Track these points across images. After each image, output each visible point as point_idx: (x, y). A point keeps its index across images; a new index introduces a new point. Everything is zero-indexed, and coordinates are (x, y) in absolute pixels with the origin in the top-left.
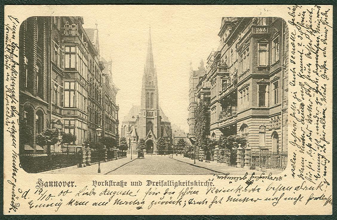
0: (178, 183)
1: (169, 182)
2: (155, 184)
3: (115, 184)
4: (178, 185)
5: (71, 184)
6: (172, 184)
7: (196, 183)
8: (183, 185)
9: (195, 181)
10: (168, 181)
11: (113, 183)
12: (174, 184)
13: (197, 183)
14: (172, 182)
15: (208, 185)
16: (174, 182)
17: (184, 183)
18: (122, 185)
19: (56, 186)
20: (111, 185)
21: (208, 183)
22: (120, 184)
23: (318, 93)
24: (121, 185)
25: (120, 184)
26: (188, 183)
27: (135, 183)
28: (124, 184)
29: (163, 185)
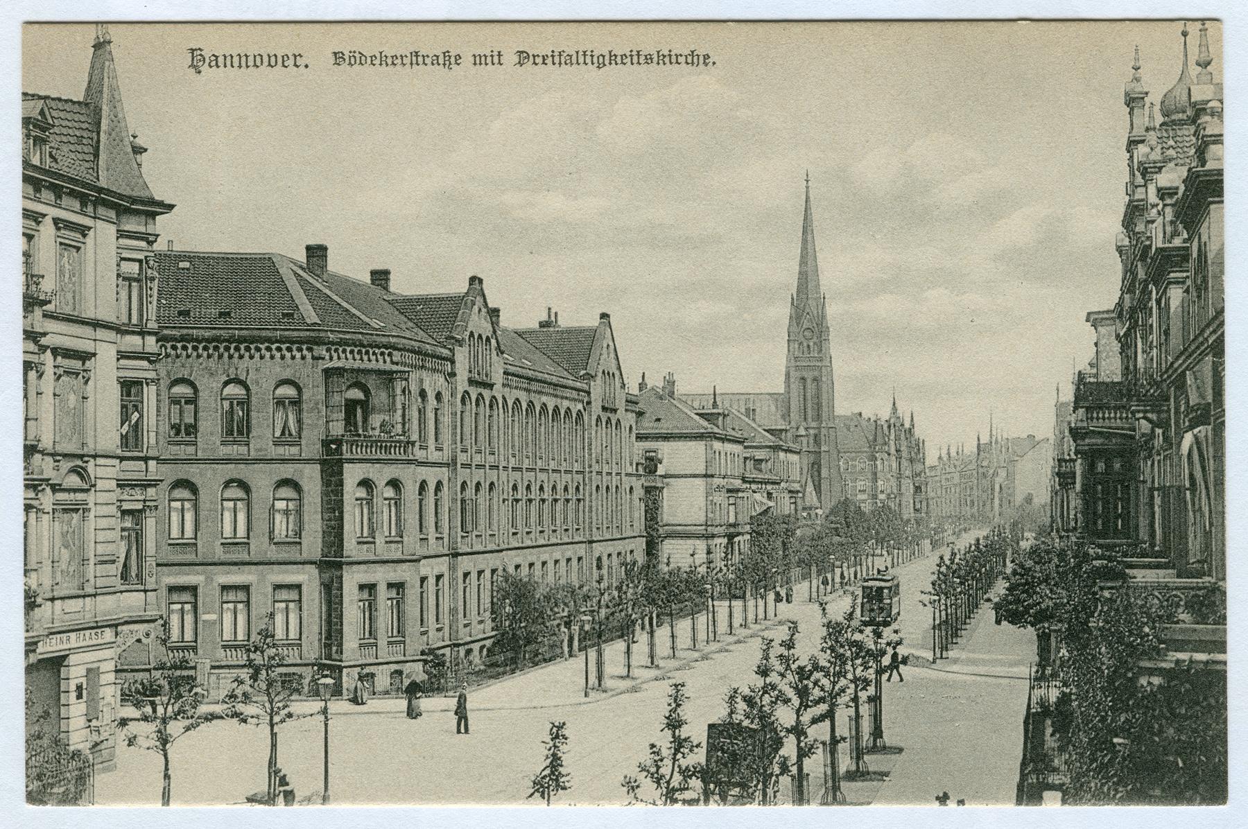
0: (607, 58)
1: (581, 53)
2: (539, 60)
3: (428, 61)
4: (607, 62)
5: (290, 62)
6: (588, 60)
7: (384, 59)
8: (622, 63)
9: (658, 52)
10: (577, 52)
11: (420, 59)
12: (595, 60)
13: (386, 57)
14: (589, 53)
15: (695, 61)
16: (596, 53)
17: (286, 58)
18: (447, 63)
19: (557, 65)
20: (414, 62)
21: (696, 58)
22: (441, 61)
23: (710, 656)
24: (444, 64)
25: (441, 61)
26: (635, 58)
27: (236, 59)
28: (453, 60)
29: (563, 62)
